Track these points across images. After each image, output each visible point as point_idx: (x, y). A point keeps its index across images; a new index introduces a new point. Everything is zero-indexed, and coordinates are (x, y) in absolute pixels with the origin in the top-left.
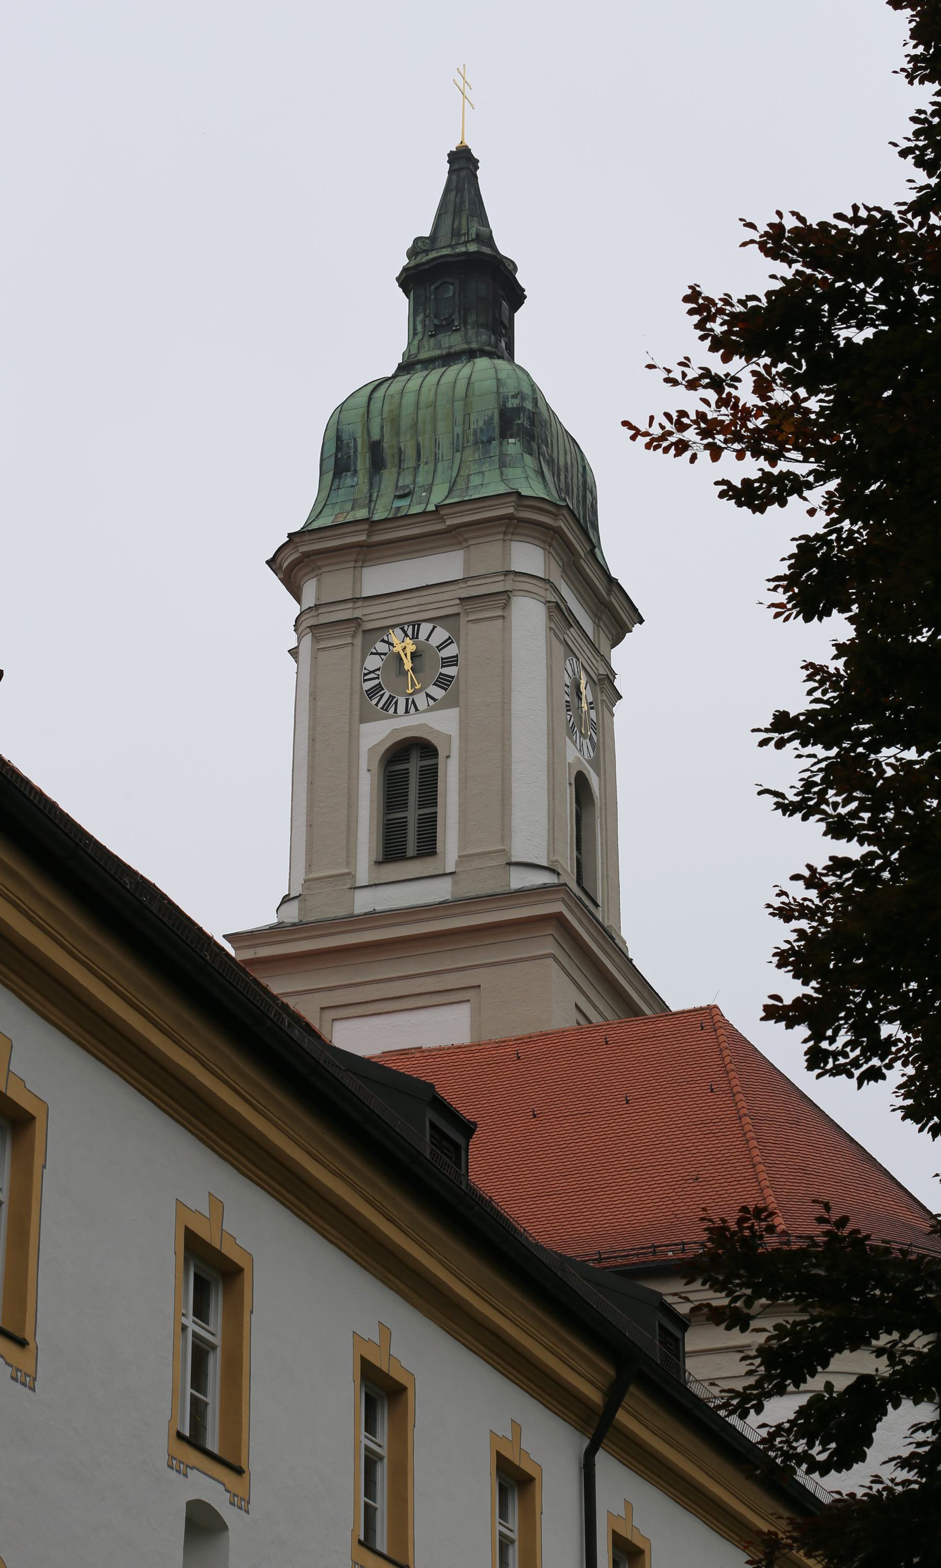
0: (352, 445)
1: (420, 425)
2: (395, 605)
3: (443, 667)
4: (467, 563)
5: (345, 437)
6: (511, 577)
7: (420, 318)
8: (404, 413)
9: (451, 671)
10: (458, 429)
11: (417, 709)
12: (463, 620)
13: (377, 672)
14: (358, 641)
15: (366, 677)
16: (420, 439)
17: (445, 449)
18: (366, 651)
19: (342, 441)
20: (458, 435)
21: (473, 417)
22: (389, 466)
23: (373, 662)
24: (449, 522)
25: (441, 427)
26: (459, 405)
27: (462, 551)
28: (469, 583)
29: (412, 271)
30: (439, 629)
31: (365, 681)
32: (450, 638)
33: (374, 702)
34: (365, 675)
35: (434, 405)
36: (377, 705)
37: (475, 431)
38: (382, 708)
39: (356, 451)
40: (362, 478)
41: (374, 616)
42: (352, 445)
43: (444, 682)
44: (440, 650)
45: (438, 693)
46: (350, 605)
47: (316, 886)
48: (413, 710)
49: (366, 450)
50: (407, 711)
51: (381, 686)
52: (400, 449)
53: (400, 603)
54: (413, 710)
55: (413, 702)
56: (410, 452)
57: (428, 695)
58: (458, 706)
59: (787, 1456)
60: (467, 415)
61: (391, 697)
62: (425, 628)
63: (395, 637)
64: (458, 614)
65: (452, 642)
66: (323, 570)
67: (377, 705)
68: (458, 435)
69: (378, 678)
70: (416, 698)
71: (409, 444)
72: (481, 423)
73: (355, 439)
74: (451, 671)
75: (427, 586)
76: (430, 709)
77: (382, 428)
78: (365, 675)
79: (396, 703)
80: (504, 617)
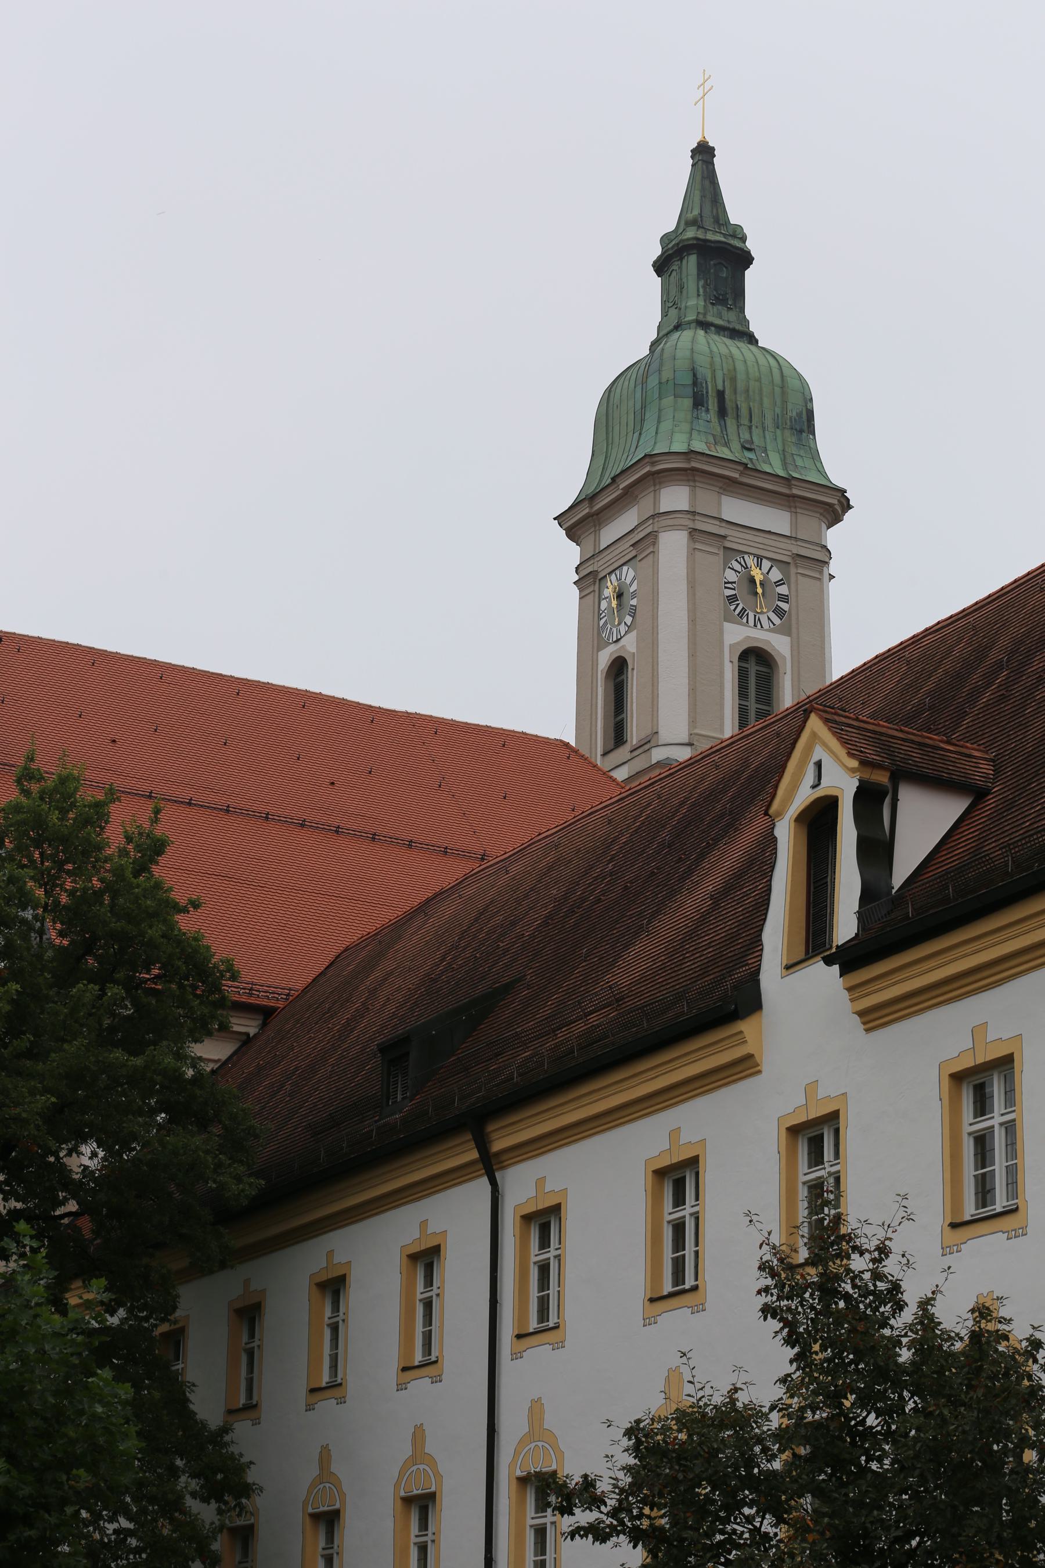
0: (704, 385)
1: (751, 393)
2: (747, 537)
3: (778, 600)
4: (794, 525)
5: (699, 376)
6: (824, 550)
7: (701, 283)
8: (739, 377)
9: (785, 606)
10: (778, 410)
11: (762, 627)
12: (793, 570)
13: (739, 560)
14: (721, 552)
15: (726, 585)
16: (751, 404)
17: (769, 422)
18: (726, 565)
19: (697, 379)
20: (778, 415)
21: (790, 406)
22: (729, 416)
23: (731, 576)
24: (795, 491)
25: (766, 402)
26: (777, 390)
27: (688, 488)
28: (799, 543)
29: (700, 243)
30: (774, 568)
31: (726, 588)
32: (782, 580)
33: (733, 607)
34: (725, 583)
35: (759, 380)
36: (734, 610)
37: (791, 418)
38: (738, 615)
39: (707, 392)
40: (713, 415)
41: (736, 539)
42: (704, 385)
43: (779, 612)
44: (777, 586)
45: (777, 621)
46: (718, 523)
47: (704, 741)
48: (759, 626)
49: (715, 394)
50: (755, 625)
51: (737, 597)
52: (737, 406)
53: (750, 536)
54: (759, 626)
55: (759, 619)
56: (744, 412)
57: (769, 618)
58: (789, 634)
59: (796, 1481)
60: (785, 402)
61: (743, 610)
62: (767, 565)
63: (751, 561)
64: (789, 563)
65: (784, 584)
66: (698, 484)
67: (734, 610)
68: (778, 415)
69: (734, 589)
70: (761, 617)
71: (743, 405)
72: (794, 414)
73: (706, 382)
74: (785, 606)
75: (770, 532)
76: (770, 630)
77: (724, 382)
78: (725, 583)
79: (748, 614)
80: (653, 552)
